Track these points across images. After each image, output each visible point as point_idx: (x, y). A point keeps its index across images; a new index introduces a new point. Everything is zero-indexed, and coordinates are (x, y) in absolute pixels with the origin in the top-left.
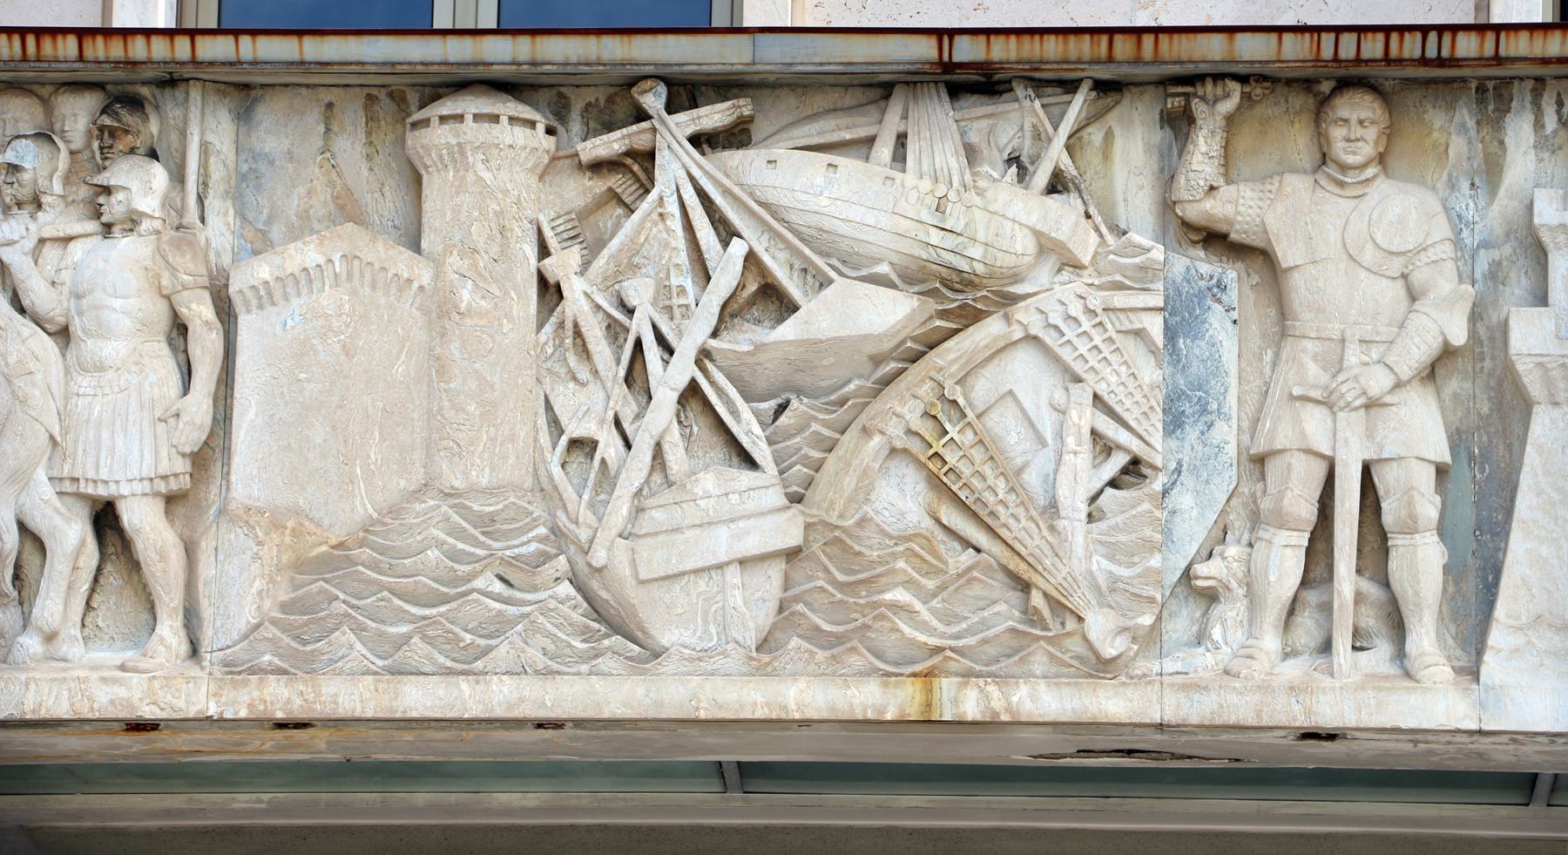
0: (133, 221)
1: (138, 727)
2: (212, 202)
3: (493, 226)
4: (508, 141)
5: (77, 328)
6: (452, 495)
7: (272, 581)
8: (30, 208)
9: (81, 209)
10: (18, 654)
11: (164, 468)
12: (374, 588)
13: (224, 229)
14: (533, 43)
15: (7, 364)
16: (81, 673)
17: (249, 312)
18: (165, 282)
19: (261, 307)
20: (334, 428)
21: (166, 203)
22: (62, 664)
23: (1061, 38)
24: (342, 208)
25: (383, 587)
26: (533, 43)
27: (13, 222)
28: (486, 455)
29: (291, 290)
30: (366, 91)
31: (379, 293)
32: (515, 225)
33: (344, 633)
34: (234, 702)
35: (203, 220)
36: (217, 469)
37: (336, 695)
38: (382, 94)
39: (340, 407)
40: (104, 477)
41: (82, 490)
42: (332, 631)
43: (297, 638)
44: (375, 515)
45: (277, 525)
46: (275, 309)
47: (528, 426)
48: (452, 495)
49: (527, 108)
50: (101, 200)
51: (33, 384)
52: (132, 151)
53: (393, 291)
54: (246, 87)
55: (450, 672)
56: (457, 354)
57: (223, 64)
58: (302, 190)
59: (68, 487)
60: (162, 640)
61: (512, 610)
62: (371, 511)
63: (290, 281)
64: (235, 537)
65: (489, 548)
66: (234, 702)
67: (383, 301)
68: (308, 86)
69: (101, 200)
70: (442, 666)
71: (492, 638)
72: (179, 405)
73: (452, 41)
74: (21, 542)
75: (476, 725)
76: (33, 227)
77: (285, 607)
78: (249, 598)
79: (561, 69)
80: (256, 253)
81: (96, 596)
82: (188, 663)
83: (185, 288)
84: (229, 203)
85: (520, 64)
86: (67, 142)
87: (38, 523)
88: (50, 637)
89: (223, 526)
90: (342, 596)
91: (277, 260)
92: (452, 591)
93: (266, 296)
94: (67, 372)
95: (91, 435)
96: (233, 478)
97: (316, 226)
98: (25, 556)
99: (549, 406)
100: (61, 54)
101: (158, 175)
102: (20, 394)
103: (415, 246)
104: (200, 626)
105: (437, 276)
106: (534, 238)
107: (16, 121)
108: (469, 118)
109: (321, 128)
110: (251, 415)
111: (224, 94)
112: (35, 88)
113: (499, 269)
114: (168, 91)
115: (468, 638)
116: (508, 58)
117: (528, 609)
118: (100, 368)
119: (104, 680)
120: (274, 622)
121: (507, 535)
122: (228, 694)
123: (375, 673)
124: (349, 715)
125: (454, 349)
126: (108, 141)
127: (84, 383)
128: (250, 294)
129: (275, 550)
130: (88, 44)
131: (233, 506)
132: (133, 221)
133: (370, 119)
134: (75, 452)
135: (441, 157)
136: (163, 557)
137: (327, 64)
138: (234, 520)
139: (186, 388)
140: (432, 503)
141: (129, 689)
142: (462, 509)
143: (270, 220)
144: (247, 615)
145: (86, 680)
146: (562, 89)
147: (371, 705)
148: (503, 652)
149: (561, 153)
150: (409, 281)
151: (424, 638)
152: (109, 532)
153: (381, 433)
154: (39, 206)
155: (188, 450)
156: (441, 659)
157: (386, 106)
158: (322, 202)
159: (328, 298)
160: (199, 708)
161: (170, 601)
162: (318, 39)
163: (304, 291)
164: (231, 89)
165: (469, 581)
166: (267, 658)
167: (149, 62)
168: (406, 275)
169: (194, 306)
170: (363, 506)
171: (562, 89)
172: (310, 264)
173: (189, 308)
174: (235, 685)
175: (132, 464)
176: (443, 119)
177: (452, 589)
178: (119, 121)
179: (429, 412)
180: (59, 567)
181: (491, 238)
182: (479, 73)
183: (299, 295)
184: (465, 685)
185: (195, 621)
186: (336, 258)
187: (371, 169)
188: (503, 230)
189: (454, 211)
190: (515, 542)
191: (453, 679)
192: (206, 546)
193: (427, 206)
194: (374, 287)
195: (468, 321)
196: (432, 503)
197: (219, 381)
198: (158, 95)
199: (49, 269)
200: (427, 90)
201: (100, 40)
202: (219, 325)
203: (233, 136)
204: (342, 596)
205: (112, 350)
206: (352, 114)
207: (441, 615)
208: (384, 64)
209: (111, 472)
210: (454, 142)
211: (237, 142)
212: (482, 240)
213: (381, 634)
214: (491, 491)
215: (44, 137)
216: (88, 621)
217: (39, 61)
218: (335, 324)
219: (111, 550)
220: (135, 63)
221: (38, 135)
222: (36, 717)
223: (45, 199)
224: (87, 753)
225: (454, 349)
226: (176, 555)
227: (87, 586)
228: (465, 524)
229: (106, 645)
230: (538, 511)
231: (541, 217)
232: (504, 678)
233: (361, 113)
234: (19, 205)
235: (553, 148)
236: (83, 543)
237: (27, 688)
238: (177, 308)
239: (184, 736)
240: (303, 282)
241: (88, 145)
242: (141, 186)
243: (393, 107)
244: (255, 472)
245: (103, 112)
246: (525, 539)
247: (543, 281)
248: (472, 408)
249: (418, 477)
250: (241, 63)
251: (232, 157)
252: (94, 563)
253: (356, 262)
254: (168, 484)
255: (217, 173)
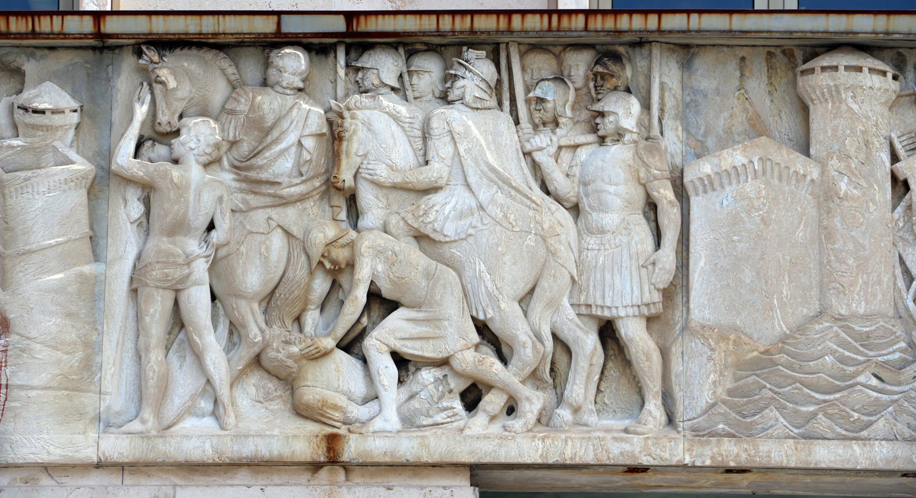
0: (619, 135)
1: (634, 470)
2: (668, 123)
3: (860, 140)
4: (869, 84)
5: (585, 204)
6: (840, 320)
7: (721, 374)
8: (551, 126)
9: (583, 127)
10: (556, 421)
11: (647, 298)
12: (789, 381)
13: (675, 139)
14: (888, 20)
15: (543, 229)
16: (601, 434)
17: (697, 195)
18: (642, 175)
19: (705, 192)
20: (758, 273)
21: (640, 123)
22: (585, 428)
23: (418, 17)
24: (753, 126)
25: (796, 380)
26: (888, 20)
27: (542, 136)
28: (862, 294)
29: (725, 181)
30: (767, 49)
31: (784, 183)
32: (875, 140)
33: (772, 411)
34: (702, 455)
35: (662, 133)
36: (679, 299)
37: (769, 452)
38: (778, 51)
39: (762, 259)
40: (609, 304)
41: (594, 313)
42: (763, 409)
43: (739, 413)
44: (788, 332)
45: (723, 338)
46: (715, 193)
47: (886, 275)
48: (840, 320)
49: (881, 63)
50: (598, 120)
51: (560, 242)
52: (616, 88)
53: (794, 182)
54: (687, 46)
55: (845, 438)
56: (839, 225)
57: (678, 32)
58: (726, 114)
59: (584, 310)
60: (650, 413)
61: (885, 397)
62: (785, 329)
63: (724, 175)
64: (696, 345)
65: (866, 355)
66: (702, 455)
67: (787, 189)
68: (728, 46)
69: (598, 120)
70: (839, 434)
71: (871, 415)
72: (654, 257)
73: (765, 17)
74: (554, 347)
75: (862, 473)
76: (555, 139)
77: (730, 392)
78: (707, 386)
79: (906, 37)
80: (698, 156)
81: (603, 383)
82: (667, 429)
83: (656, 178)
84: (678, 122)
85: (877, 33)
86: (573, 83)
87: (567, 334)
88: (576, 410)
89: (687, 338)
90: (768, 386)
91: (716, 161)
92: (843, 384)
93: (709, 185)
94: (579, 234)
95: (598, 276)
96: (692, 306)
97: (736, 138)
98: (557, 356)
99: (902, 262)
100: (573, 26)
101: (635, 105)
102: (552, 249)
103: (806, 152)
104: (674, 404)
105: (823, 173)
106: (887, 149)
107: (540, 69)
108: (841, 68)
109: (738, 74)
110: (702, 263)
111: (673, 51)
112: (550, 48)
113: (866, 169)
114: (637, 50)
115: (856, 415)
116: (870, 29)
117: (896, 397)
118: (602, 231)
119: (615, 439)
120: (724, 402)
121: (878, 347)
122: (697, 449)
123: (794, 438)
124: (779, 465)
125: (837, 222)
126: (600, 82)
127: (592, 241)
128: (698, 183)
129: (723, 354)
130: (591, 20)
131: (693, 324)
132: (619, 135)
133: (770, 68)
134: (588, 286)
135: (823, 93)
136: (649, 358)
137: (747, 32)
138: (694, 333)
139: (658, 244)
140: (827, 324)
141: (632, 445)
142: (847, 329)
143: (705, 135)
144: (705, 398)
145: (604, 439)
146: (900, 50)
147: (794, 458)
148: (881, 425)
149: (903, 93)
150: (804, 176)
151: (826, 415)
152: (609, 340)
153: (789, 277)
154: (557, 124)
155: (661, 286)
156: (839, 430)
157: (780, 60)
158: (740, 123)
159: (750, 187)
160: (678, 458)
161: (653, 387)
162: (742, 16)
163: (734, 182)
164: (677, 48)
165: (854, 377)
166: (721, 426)
167: (630, 31)
168: (802, 172)
169: (662, 191)
170: (780, 326)
171: (900, 50)
172: (738, 164)
173: (659, 193)
174: (702, 444)
175: (626, 294)
176: (824, 69)
177: (843, 382)
178: (608, 69)
179: (821, 263)
180: (582, 364)
181: (858, 148)
182: (850, 38)
183: (730, 184)
184: (856, 448)
185: (669, 401)
186: (756, 160)
187: (772, 101)
188: (867, 143)
189: (833, 130)
190: (884, 352)
191: (848, 443)
192: (676, 350)
193: (814, 126)
194: (780, 179)
195: (846, 203)
196: (827, 324)
197: (679, 241)
198: (631, 52)
199: (565, 166)
200: (808, 49)
201: (599, 17)
202: (678, 204)
203: (680, 79)
204: (768, 386)
205: (610, 220)
206: (758, 65)
207: (836, 399)
208: (786, 32)
209: (613, 301)
210: (832, 84)
211: (682, 82)
212: (853, 150)
213: (797, 412)
214: (867, 317)
215: (559, 79)
216: (598, 399)
217: (559, 31)
218: (756, 204)
219: (611, 352)
220: (621, 32)
221: (555, 79)
222: (573, 462)
223: (562, 120)
224: (585, 486)
225: (837, 222)
226: (656, 357)
227: (597, 377)
228: (849, 339)
229: (611, 416)
230: (899, 331)
231: (893, 135)
232: (883, 442)
233: (764, 64)
234: (544, 124)
235: (898, 89)
236: (595, 349)
237: (566, 444)
238: (650, 192)
239: (660, 476)
240: (733, 176)
241: (586, 85)
242: (625, 112)
243: (785, 60)
244: (706, 302)
245: (597, 63)
246: (891, 350)
247: (894, 178)
248: (851, 261)
249: (815, 307)
250: (689, 31)
251: (679, 92)
252: (602, 361)
253: (768, 163)
254: (649, 309)
255: (670, 103)
